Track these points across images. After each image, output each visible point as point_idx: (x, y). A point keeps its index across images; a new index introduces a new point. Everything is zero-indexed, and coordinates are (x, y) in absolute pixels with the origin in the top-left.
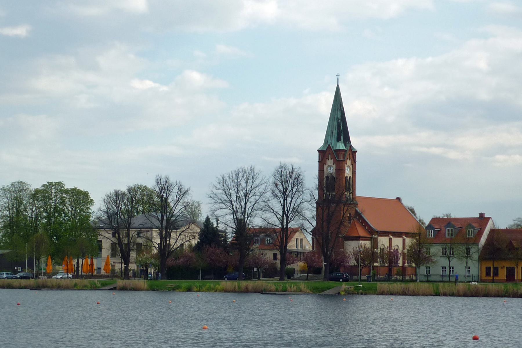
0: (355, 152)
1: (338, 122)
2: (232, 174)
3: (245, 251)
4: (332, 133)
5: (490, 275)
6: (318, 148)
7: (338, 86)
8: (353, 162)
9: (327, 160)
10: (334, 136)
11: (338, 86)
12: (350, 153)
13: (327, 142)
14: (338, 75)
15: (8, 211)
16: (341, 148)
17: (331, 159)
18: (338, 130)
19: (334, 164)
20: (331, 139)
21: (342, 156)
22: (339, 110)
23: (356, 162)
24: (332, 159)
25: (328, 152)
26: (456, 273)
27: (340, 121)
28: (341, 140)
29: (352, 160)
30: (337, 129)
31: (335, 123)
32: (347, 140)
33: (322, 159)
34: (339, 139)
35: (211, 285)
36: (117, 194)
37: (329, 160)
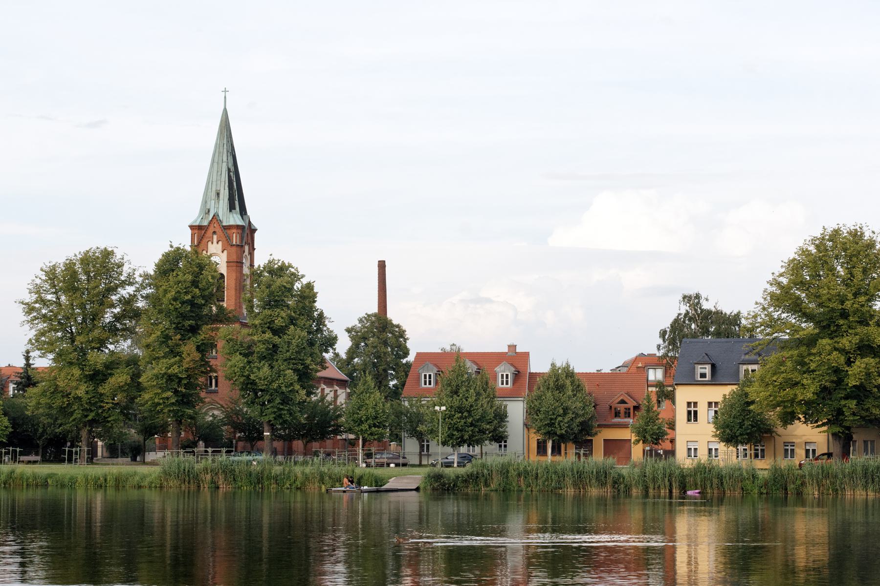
1: (229, 177)
2: (818, 426)
4: (218, 194)
5: (694, 411)
6: (190, 222)
9: (210, 243)
10: (221, 202)
12: (218, 230)
13: (209, 211)
14: (225, 91)
16: (232, 223)
17: (218, 243)
18: (229, 189)
19: (223, 252)
21: (236, 236)
22: (229, 154)
23: (255, 249)
24: (220, 243)
25: (211, 230)
26: (773, 274)
27: (232, 174)
28: (235, 209)
29: (251, 245)
30: (227, 188)
31: (223, 179)
32: (243, 211)
33: (200, 242)
34: (232, 208)
35: (316, 398)
37: (212, 243)
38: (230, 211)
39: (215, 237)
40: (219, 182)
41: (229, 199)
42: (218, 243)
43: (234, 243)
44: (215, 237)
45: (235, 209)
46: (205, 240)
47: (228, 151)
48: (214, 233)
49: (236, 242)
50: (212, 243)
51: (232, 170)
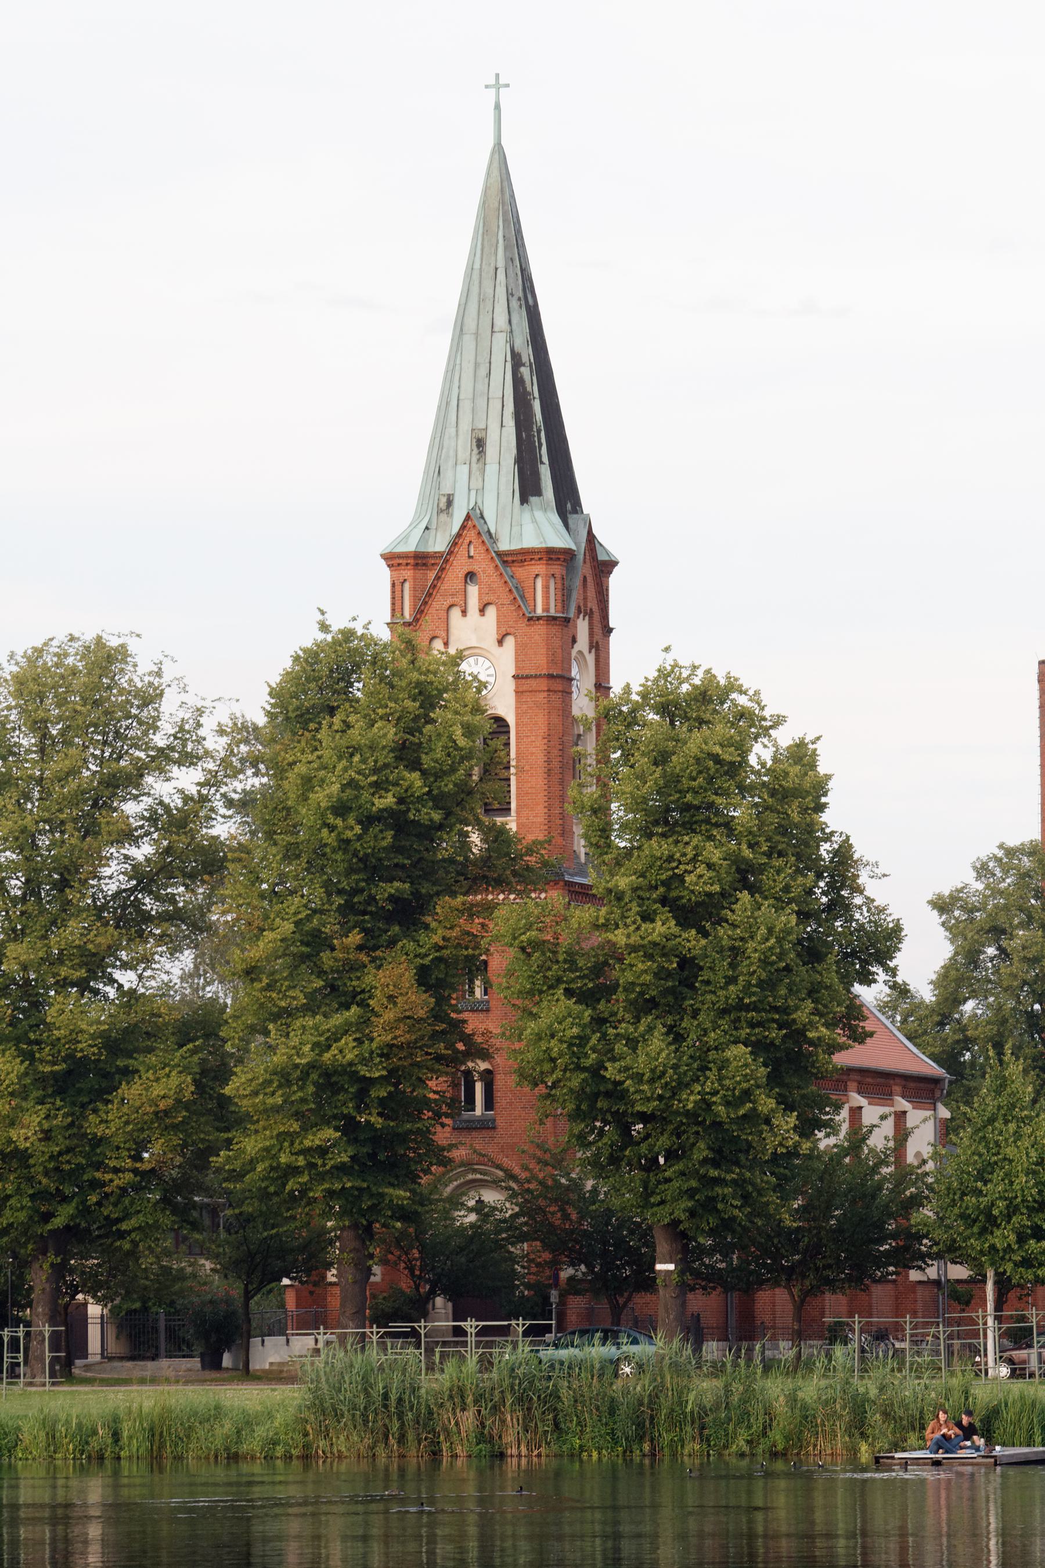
0: (610, 565)
1: (518, 382)
3: (847, 1160)
4: (480, 444)
7: (499, 153)
8: (598, 629)
9: (456, 613)
10: (491, 469)
11: (499, 153)
12: (483, 566)
13: (450, 503)
14: (498, 85)
15: (366, 855)
16: (530, 541)
17: (482, 611)
20: (476, 484)
21: (546, 588)
22: (514, 304)
23: (610, 630)
24: (491, 612)
27: (525, 371)
29: (597, 616)
33: (421, 612)
36: (820, 787)
37: (464, 613)
38: (524, 500)
39: (473, 591)
40: (482, 402)
41: (520, 460)
42: (482, 611)
43: (539, 611)
44: (473, 591)
45: (538, 492)
46: (438, 604)
47: (509, 294)
48: (470, 576)
49: (546, 609)
50: (464, 613)
51: (525, 359)
